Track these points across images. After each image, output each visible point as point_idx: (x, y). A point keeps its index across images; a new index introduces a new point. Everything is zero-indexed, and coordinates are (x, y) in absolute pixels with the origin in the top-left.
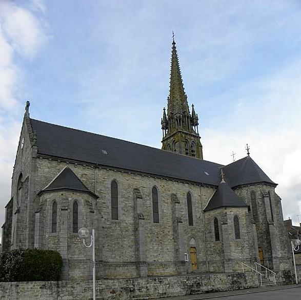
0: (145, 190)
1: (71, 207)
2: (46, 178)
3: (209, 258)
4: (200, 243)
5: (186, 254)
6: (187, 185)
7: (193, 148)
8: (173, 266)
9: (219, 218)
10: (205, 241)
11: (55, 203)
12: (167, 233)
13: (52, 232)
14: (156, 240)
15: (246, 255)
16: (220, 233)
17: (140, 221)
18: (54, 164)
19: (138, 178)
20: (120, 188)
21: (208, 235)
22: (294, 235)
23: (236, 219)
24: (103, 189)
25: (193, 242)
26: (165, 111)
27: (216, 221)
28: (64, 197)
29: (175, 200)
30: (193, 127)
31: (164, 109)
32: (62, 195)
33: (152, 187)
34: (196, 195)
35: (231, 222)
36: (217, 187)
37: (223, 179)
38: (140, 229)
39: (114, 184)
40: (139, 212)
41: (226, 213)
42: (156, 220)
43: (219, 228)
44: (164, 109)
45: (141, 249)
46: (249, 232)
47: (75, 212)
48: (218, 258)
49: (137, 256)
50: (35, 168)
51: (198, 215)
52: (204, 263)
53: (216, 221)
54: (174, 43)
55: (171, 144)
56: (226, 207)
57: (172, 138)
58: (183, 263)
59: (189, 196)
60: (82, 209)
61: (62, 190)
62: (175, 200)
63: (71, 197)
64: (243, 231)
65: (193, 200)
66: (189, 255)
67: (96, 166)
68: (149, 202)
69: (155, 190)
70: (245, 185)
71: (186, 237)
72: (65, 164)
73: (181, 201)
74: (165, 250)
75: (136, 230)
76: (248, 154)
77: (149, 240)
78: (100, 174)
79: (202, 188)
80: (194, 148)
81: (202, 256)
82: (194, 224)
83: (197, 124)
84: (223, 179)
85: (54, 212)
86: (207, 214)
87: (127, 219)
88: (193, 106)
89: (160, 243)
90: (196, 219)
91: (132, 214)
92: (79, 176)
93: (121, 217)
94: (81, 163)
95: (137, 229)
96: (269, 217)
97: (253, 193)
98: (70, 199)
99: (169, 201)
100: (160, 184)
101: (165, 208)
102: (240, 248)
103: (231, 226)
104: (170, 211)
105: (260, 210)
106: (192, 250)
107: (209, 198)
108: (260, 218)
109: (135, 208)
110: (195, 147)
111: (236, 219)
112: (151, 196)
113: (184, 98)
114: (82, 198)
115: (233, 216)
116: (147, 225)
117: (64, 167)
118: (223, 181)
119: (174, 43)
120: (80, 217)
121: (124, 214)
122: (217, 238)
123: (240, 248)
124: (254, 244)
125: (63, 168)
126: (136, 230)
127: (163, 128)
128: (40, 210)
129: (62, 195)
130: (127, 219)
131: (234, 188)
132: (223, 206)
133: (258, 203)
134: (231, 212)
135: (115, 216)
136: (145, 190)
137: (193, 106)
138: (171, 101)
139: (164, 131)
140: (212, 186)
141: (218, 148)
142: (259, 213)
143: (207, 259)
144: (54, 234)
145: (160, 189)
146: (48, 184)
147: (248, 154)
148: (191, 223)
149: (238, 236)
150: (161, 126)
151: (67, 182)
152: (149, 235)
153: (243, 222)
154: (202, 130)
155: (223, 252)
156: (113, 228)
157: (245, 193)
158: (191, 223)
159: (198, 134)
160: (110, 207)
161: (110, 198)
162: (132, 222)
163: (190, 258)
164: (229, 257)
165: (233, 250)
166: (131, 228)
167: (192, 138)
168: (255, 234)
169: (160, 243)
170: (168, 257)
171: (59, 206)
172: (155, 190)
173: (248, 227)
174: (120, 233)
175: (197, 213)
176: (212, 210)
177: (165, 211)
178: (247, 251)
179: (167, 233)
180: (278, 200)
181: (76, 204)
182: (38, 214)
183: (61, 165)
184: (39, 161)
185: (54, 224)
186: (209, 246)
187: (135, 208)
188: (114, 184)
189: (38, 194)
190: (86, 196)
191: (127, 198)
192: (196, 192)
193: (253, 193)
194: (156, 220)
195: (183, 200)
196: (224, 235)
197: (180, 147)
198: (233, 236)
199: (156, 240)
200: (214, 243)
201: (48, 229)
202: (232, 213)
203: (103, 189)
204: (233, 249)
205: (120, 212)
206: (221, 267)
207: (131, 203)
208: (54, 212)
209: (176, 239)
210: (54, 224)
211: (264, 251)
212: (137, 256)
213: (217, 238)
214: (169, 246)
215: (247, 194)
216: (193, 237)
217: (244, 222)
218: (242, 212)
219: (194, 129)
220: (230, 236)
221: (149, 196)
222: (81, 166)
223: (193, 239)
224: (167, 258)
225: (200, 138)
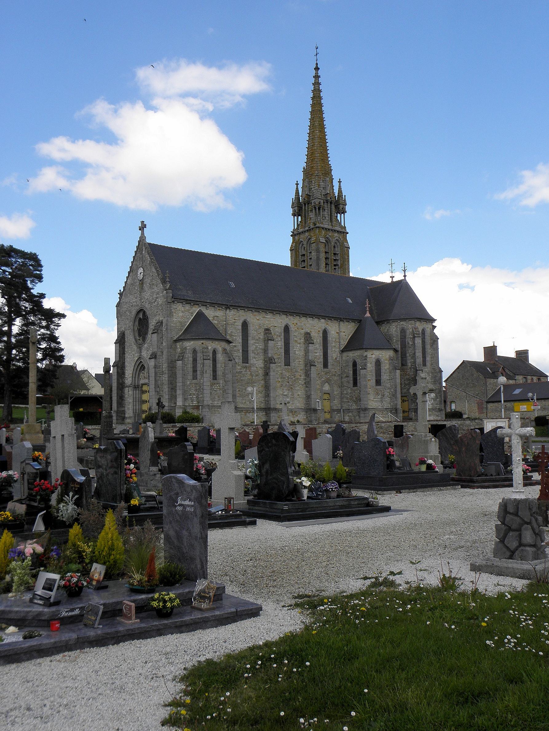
0: (277, 329)
1: (211, 355)
2: (180, 322)
3: (345, 406)
4: (336, 388)
5: (318, 400)
6: (323, 320)
7: (336, 249)
8: (303, 413)
9: (358, 361)
10: (341, 386)
11: (195, 351)
12: (299, 377)
13: (193, 379)
14: (286, 385)
15: (387, 404)
16: (358, 378)
17: (272, 365)
18: (187, 307)
19: (269, 316)
20: (252, 331)
21: (345, 380)
22: (493, 373)
23: (378, 363)
24: (234, 331)
25: (327, 387)
26: (297, 188)
27: (355, 364)
28: (203, 346)
29: (308, 338)
30: (339, 215)
31: (297, 184)
32: (202, 343)
33: (284, 326)
34: (333, 332)
35: (371, 366)
36: (360, 321)
37: (368, 312)
38: (272, 373)
39: (245, 325)
40: (270, 355)
41: (366, 356)
42: (287, 363)
43: (131, 628)
44: (297, 184)
45: (272, 395)
46: (392, 378)
47: (214, 360)
48: (354, 407)
49: (267, 402)
50: (170, 313)
51: (335, 356)
52: (338, 411)
53: (355, 364)
54: (317, 69)
55: (305, 243)
56: (367, 349)
57: (307, 234)
58: (315, 410)
59: (325, 333)
60: (220, 357)
61: (203, 339)
62: (308, 338)
63: (211, 345)
64: (385, 377)
65: (329, 339)
66: (322, 403)
67: (228, 307)
68: (280, 344)
69: (287, 329)
70: (395, 320)
71: (319, 382)
72: (197, 306)
73: (315, 341)
74: (296, 395)
75: (267, 374)
76: (405, 276)
77: (279, 385)
78: (231, 314)
79: (341, 323)
80: (338, 250)
81: (336, 403)
82: (329, 367)
83: (344, 212)
84: (368, 312)
85: (195, 360)
86: (345, 354)
87: (257, 362)
88: (340, 182)
89: (291, 388)
90: (331, 361)
91: (262, 357)
92: (211, 319)
93: (252, 361)
94: (213, 304)
95: (268, 374)
96: (419, 360)
97: (403, 331)
98: (210, 348)
99: (302, 340)
100: (293, 322)
101: (297, 350)
102: (380, 397)
103: (371, 371)
104: (302, 353)
105: (410, 352)
106: (326, 397)
107: (349, 335)
108: (409, 361)
109: (265, 351)
110: (338, 254)
111: (378, 363)
112: (282, 337)
113: (327, 172)
114: (219, 346)
115: (374, 360)
116: (277, 370)
117: (196, 310)
118: (368, 315)
119: (317, 69)
120: (218, 365)
121: (255, 358)
122: (355, 384)
123: (380, 397)
124: (396, 393)
125: (195, 311)
126: (267, 374)
127: (294, 215)
128: (182, 357)
129: (202, 343)
130: (257, 362)
131: (378, 323)
132: (363, 349)
133: (408, 343)
134: (373, 355)
135: (245, 359)
136: (277, 329)
137: (340, 182)
138: (308, 173)
139: (296, 217)
140: (354, 320)
141: (368, 264)
142: (408, 355)
143: (342, 407)
144: (194, 381)
145: (292, 328)
146: (182, 329)
147: (405, 276)
148: (325, 365)
149: (378, 382)
150: (291, 211)
151: (200, 328)
152: (279, 380)
153: (385, 367)
154: (350, 220)
155: (360, 400)
156: (244, 373)
157: (394, 329)
158: (325, 365)
159: (345, 227)
160: (241, 351)
161: (241, 341)
162: (262, 365)
163: (322, 406)
164: (366, 406)
165: (372, 399)
166: (261, 372)
167: (336, 234)
168: (398, 381)
169: (291, 388)
170: (299, 403)
171: (199, 355)
172: (287, 329)
173: (390, 372)
174: (250, 377)
175: (334, 353)
176: (351, 350)
177: (297, 353)
178: (388, 399)
179: (299, 377)
180: (435, 339)
181: (214, 352)
182: (179, 363)
183: (194, 308)
184: (174, 306)
185: (195, 371)
186: (345, 392)
187: (265, 351)
188: (245, 325)
189: (175, 341)
190: (224, 344)
191: (257, 340)
192: (333, 328)
193: (403, 331)
194: (287, 363)
195: (317, 338)
196: (361, 382)
197: (318, 251)
198: (373, 382)
199: (286, 385)
200: (352, 390)
201: (190, 377)
202: (374, 356)
203: (234, 331)
204: (371, 397)
205: (251, 355)
206: (357, 417)
207: (261, 346)
208: (195, 360)
209: (308, 384)
210: (195, 371)
211: (410, 400)
212: (267, 402)
213: (355, 384)
214: (300, 391)
215: (395, 331)
216: (328, 381)
217: (387, 366)
218: (385, 355)
219: (339, 218)
220: (369, 383)
221: (280, 336)
222: (212, 308)
223: (327, 384)
224: (298, 404)
225: (348, 233)
